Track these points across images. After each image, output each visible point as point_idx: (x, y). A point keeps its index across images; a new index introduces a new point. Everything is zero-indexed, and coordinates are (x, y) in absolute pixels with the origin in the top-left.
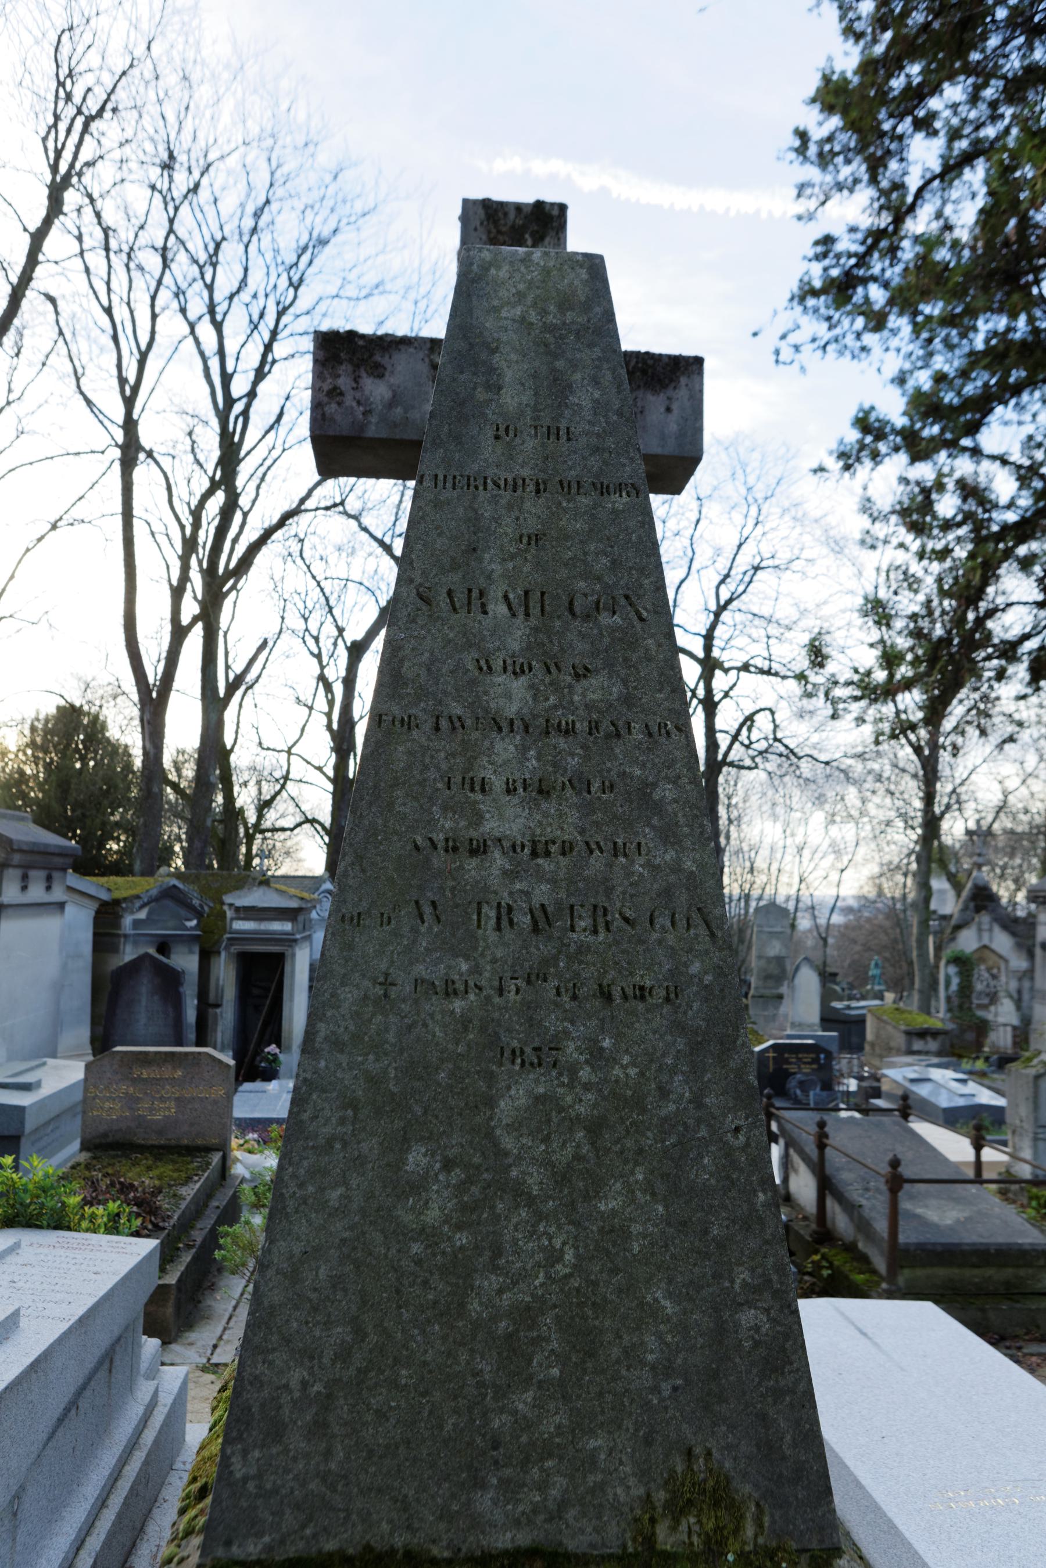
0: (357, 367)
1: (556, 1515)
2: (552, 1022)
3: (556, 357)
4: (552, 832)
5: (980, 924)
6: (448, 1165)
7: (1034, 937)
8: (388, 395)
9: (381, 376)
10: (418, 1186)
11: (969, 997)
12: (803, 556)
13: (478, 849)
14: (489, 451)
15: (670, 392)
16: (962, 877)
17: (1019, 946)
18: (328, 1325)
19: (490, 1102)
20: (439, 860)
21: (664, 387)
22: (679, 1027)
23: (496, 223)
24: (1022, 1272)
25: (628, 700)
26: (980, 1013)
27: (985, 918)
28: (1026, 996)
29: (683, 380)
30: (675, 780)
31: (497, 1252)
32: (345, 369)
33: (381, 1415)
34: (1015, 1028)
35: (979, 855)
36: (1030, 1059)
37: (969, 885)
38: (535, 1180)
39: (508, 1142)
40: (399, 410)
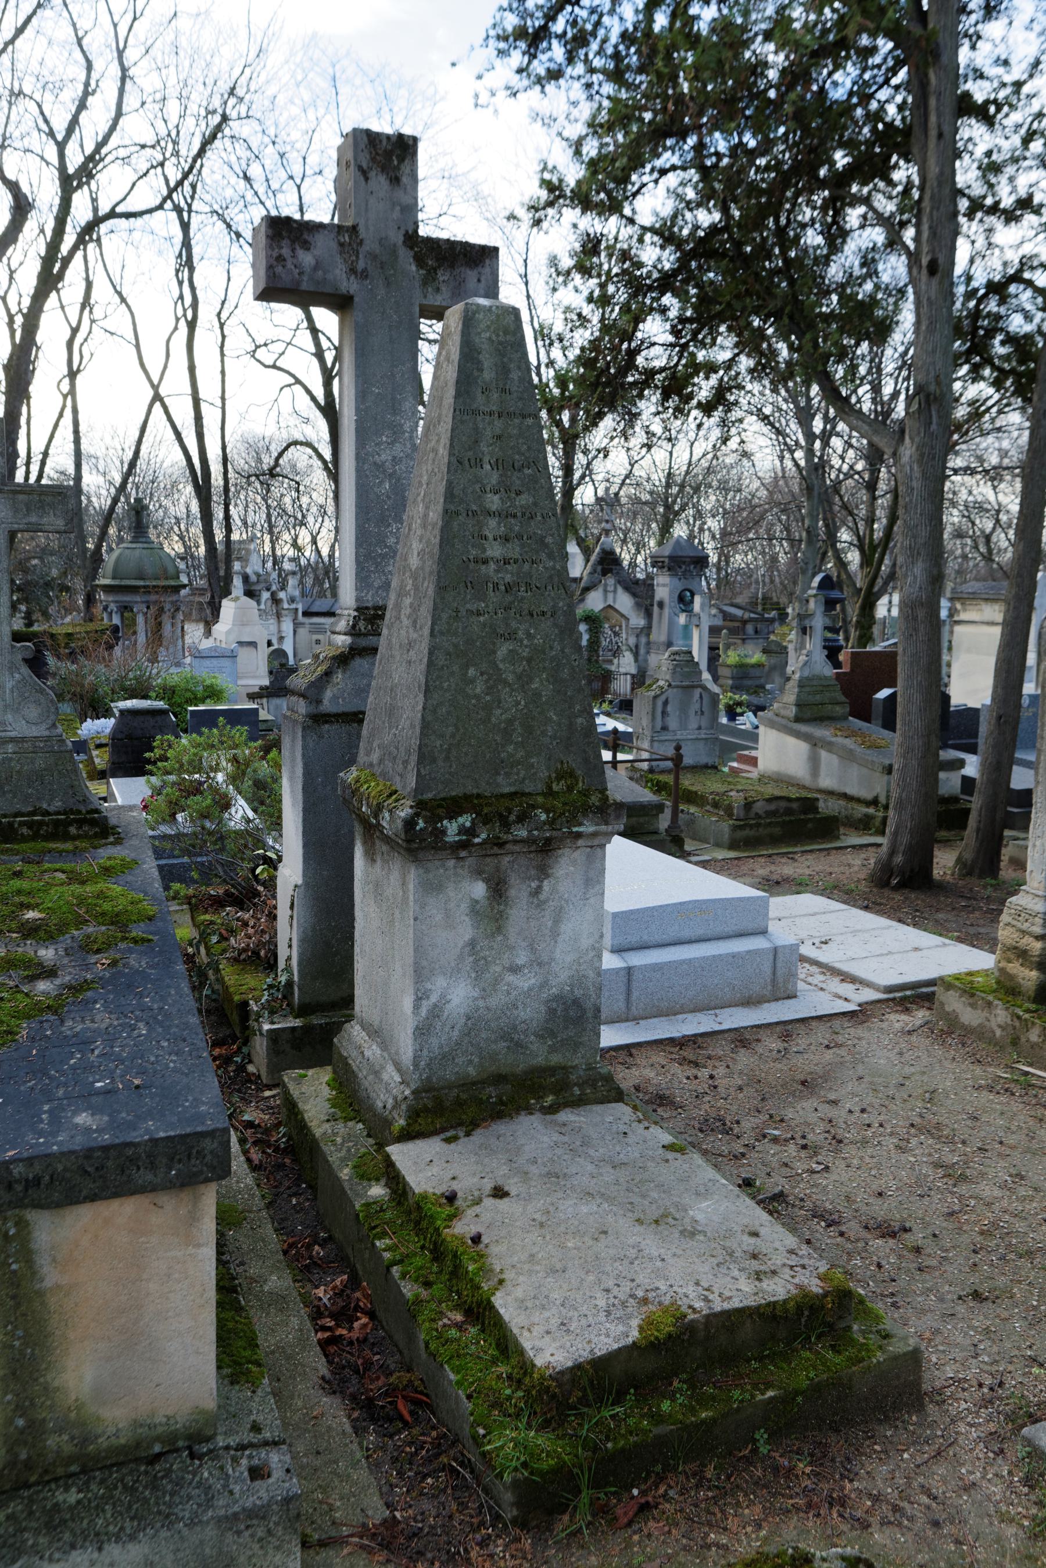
0: (293, 242)
1: (523, 781)
2: (514, 624)
3: (504, 356)
4: (510, 555)
5: (606, 585)
6: (482, 674)
7: (653, 597)
8: (313, 262)
9: (308, 249)
10: (472, 681)
11: (597, 651)
12: (450, 212)
13: (485, 562)
14: (480, 399)
15: (480, 269)
16: (591, 541)
17: (638, 605)
18: (447, 727)
19: (495, 652)
20: (472, 565)
21: (477, 265)
22: (555, 625)
23: (374, 147)
24: (641, 820)
25: (535, 504)
26: (605, 666)
27: (610, 581)
28: (642, 651)
29: (487, 262)
30: (552, 535)
31: (500, 702)
32: (286, 243)
33: (466, 754)
34: (633, 676)
35: (607, 521)
36: (650, 686)
37: (597, 550)
38: (511, 678)
39: (501, 666)
40: (320, 273)
